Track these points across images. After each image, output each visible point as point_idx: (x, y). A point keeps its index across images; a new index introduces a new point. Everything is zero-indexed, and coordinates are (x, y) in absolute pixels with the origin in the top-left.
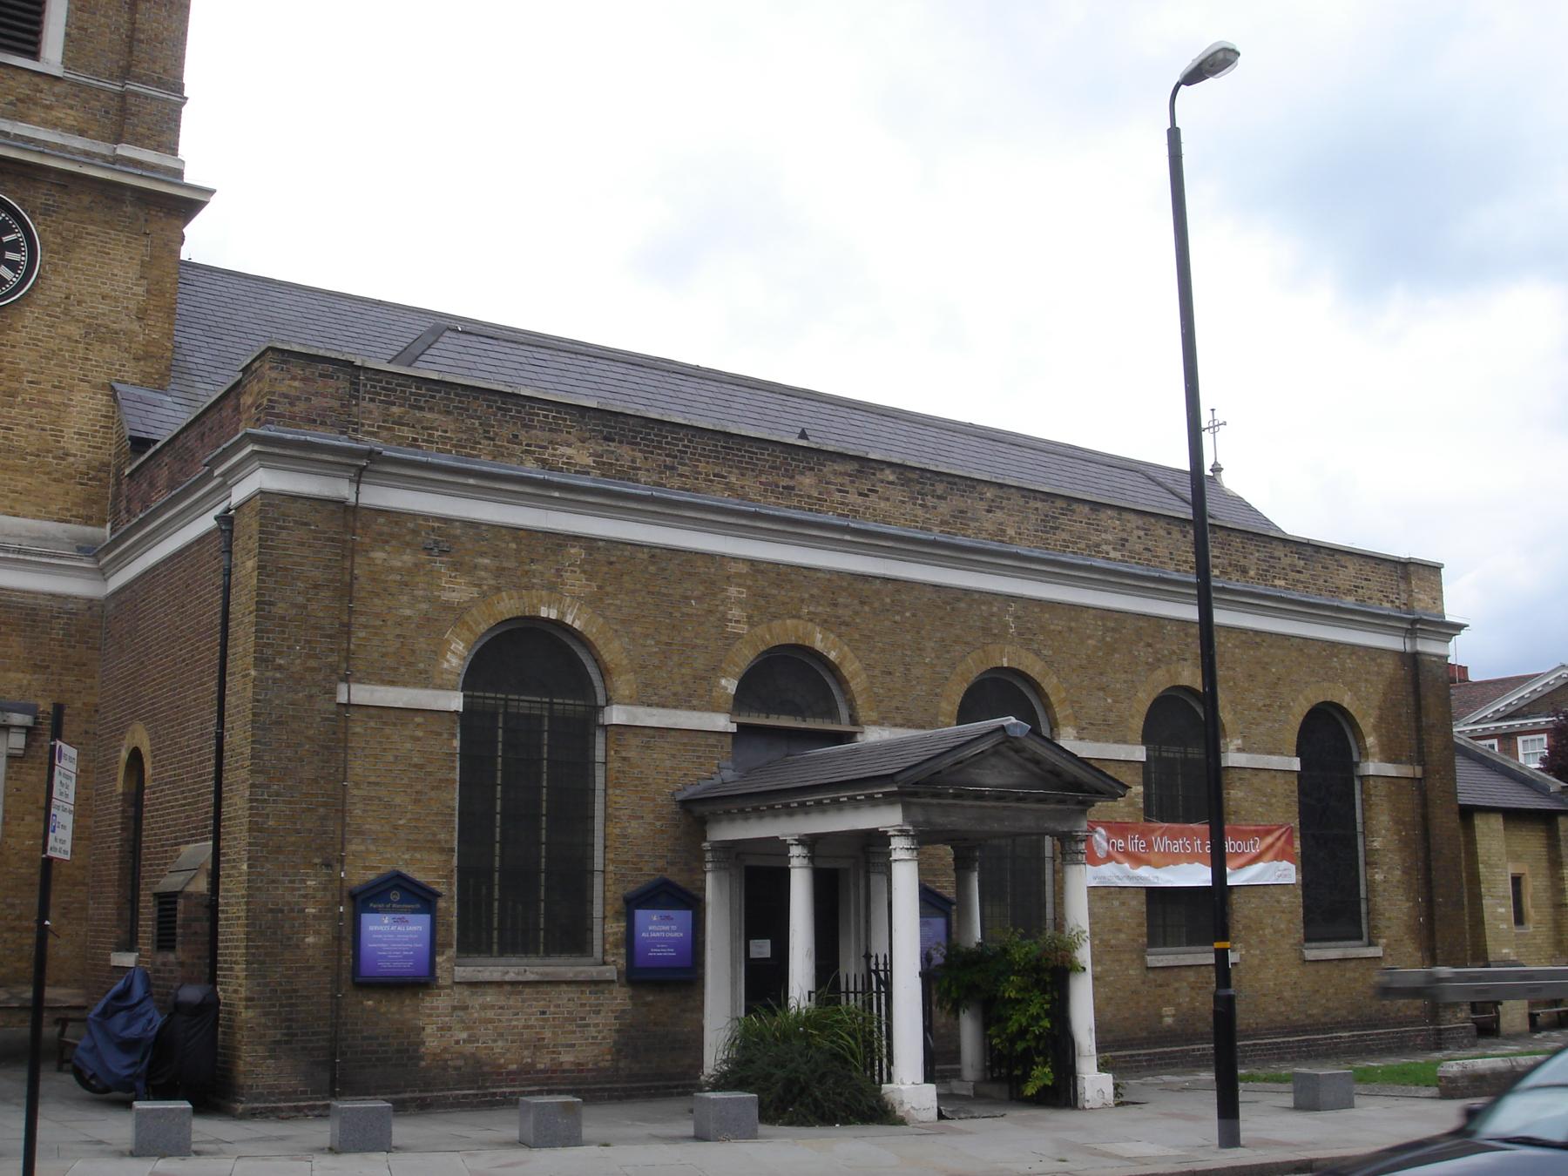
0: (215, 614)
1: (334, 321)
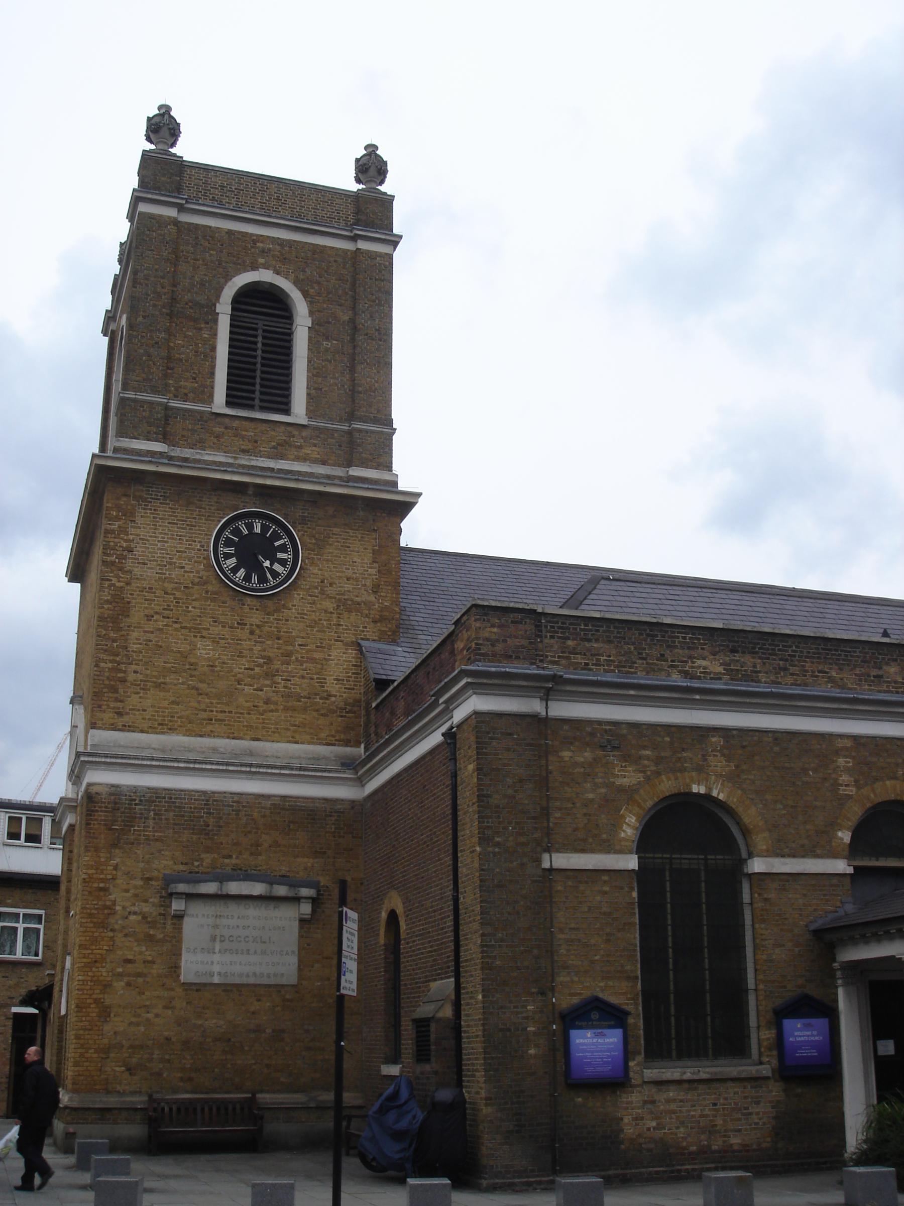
0: (447, 806)
1: (515, 580)
